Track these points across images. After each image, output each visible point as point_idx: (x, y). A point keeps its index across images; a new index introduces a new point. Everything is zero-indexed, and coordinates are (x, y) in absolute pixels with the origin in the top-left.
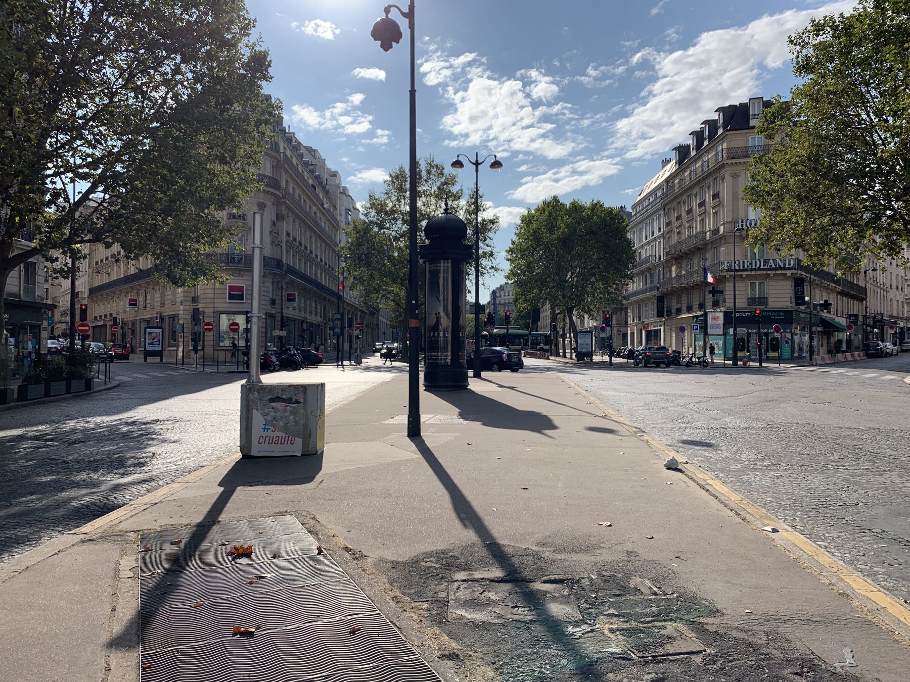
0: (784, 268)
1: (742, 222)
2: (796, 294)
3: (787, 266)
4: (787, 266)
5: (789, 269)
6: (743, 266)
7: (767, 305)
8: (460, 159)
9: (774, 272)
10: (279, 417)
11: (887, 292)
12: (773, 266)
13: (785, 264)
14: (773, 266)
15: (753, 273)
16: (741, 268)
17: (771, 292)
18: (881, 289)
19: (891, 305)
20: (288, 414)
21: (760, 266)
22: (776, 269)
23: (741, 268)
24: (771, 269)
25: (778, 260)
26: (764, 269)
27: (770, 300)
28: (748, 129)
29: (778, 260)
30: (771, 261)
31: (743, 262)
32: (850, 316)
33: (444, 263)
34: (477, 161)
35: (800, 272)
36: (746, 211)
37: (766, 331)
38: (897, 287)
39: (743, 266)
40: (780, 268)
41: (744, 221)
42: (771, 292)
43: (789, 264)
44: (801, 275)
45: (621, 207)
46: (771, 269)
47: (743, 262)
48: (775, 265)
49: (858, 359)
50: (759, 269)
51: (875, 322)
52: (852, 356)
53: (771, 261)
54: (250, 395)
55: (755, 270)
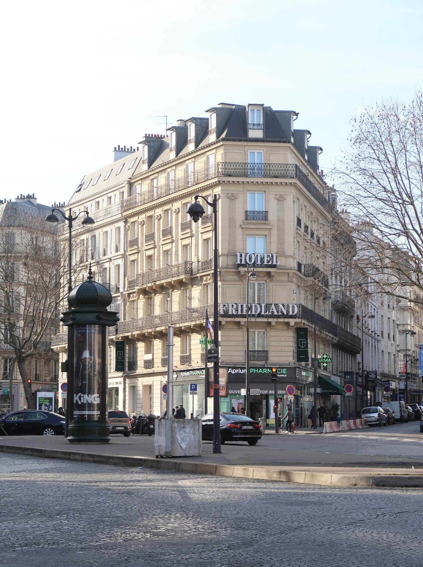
0: (288, 316)
1: (241, 256)
2: (298, 347)
3: (291, 313)
4: (291, 313)
5: (292, 317)
6: (242, 311)
7: (267, 359)
8: (55, 214)
9: (275, 320)
10: (187, 436)
11: (378, 341)
12: (276, 313)
13: (288, 311)
14: (276, 313)
15: (253, 320)
16: (240, 313)
17: (272, 344)
18: (372, 338)
19: (383, 358)
20: (190, 435)
21: (261, 311)
22: (278, 317)
23: (240, 313)
24: (273, 316)
25: (281, 306)
26: (263, 316)
27: (271, 354)
28: (245, 141)
29: (281, 306)
30: (273, 306)
31: (242, 306)
32: (346, 373)
33: (89, 327)
34: (70, 216)
35: (303, 321)
36: (244, 242)
37: (266, 392)
38: (389, 335)
39: (242, 311)
40: (283, 316)
41: (243, 255)
42: (272, 344)
43: (293, 312)
44: (304, 324)
45: (29, 197)
46: (273, 316)
47: (242, 306)
48: (278, 312)
49: (361, 427)
50: (259, 315)
51: (367, 381)
52: (355, 423)
53: (273, 306)
54: (173, 424)
55: (254, 316)
